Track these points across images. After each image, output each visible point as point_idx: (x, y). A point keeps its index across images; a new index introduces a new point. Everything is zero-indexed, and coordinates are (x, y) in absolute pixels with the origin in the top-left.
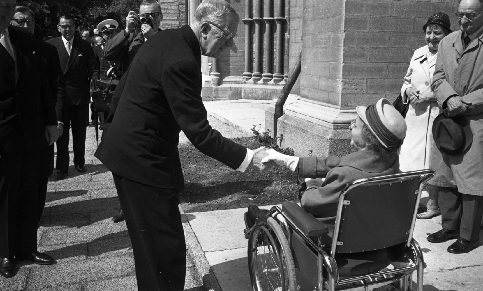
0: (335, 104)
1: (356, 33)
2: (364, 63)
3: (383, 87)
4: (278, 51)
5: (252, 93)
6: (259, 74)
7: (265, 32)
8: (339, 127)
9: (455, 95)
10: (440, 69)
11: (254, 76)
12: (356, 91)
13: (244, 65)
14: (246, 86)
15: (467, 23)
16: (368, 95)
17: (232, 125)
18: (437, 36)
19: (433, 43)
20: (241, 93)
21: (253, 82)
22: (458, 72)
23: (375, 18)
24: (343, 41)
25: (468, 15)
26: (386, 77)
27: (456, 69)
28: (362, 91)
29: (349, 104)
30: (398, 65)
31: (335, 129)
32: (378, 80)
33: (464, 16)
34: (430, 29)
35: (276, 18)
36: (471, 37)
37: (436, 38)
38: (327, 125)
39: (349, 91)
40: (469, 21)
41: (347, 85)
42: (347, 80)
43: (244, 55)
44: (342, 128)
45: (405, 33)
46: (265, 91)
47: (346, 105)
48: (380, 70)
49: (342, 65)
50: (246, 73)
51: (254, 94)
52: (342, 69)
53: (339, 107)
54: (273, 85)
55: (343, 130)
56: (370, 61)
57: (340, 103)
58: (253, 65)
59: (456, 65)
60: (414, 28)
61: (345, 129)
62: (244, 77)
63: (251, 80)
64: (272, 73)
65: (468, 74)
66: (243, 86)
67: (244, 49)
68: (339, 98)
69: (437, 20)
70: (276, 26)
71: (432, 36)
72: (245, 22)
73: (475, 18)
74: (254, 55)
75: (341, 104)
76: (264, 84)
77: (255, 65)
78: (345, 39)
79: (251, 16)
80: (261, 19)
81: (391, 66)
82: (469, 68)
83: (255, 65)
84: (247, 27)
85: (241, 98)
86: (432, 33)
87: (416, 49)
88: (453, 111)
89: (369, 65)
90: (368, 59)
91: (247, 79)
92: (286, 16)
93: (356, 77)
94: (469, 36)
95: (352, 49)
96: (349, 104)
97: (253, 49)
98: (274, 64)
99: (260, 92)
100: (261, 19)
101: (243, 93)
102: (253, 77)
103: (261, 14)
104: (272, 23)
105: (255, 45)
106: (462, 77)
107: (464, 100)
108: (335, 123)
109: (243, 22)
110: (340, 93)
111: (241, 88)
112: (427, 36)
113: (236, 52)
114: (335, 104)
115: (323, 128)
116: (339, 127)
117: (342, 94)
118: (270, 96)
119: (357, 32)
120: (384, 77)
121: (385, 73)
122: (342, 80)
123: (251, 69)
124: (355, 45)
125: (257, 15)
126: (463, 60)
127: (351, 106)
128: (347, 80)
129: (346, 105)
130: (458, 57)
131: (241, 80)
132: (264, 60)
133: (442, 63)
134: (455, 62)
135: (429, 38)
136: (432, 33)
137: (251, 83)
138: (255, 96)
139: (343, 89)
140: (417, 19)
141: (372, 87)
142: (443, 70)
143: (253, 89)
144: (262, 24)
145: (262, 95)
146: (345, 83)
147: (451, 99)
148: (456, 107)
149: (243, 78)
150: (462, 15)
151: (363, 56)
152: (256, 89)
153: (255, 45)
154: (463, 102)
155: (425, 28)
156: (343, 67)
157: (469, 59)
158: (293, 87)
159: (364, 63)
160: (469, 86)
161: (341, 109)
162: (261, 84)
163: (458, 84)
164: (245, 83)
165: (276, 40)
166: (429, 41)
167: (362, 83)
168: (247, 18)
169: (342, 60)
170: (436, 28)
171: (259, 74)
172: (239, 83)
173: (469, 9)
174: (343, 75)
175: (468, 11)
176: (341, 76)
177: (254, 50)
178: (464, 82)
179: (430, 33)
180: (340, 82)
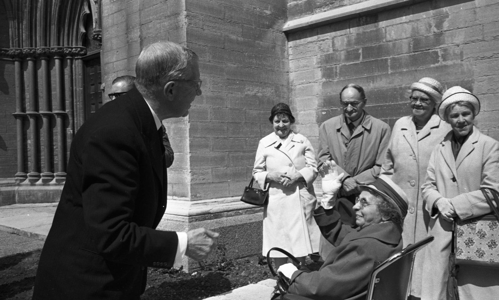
0: (183, 196)
1: (198, 123)
2: (208, 153)
3: (226, 175)
4: (59, 147)
5: (30, 195)
6: (36, 174)
7: (41, 127)
8: (194, 219)
9: (349, 177)
10: (326, 152)
11: (30, 176)
12: (203, 181)
13: (17, 165)
14: (21, 188)
15: (352, 111)
16: (214, 185)
17: (25, 234)
18: (285, 124)
19: (282, 131)
20: (14, 196)
21: (29, 183)
22: (348, 155)
23: (214, 109)
24: (188, 131)
25: (353, 104)
26: (228, 166)
27: (346, 153)
28: (209, 181)
29: (198, 195)
30: (237, 154)
31: (190, 222)
32: (222, 169)
33: (349, 105)
34: (278, 118)
35: (55, 112)
36: (355, 124)
37: (285, 126)
38: (180, 218)
39: (197, 182)
40: (354, 109)
41: (195, 176)
42: (194, 170)
43: (16, 153)
44: (197, 220)
45: (239, 123)
46: (46, 192)
47: (196, 196)
48: (222, 159)
49: (189, 156)
50: (32, 173)
51: (31, 197)
52: (189, 159)
53: (189, 198)
54: (55, 185)
55: (197, 222)
56: (213, 150)
57: (190, 194)
58: (27, 164)
59: (344, 149)
60: (246, 118)
61: (199, 221)
62: (16, 178)
63: (27, 182)
64: (53, 172)
65: (356, 157)
66: (16, 188)
67: (16, 147)
68: (187, 190)
69: (282, 110)
70: (55, 120)
71: (281, 124)
72: (16, 116)
73: (359, 105)
74: (29, 153)
75: (192, 196)
76: (44, 185)
77: (31, 164)
78: (190, 129)
79: (23, 109)
80: (36, 113)
81: (231, 155)
82: (357, 151)
83: (31, 164)
84: (18, 121)
85: (15, 203)
86: (281, 122)
87: (262, 137)
88: (350, 191)
89: (212, 154)
90: (211, 149)
91: (22, 181)
92: (67, 111)
93: (202, 167)
94: (353, 123)
95: (197, 140)
96: (198, 195)
97: (27, 146)
98: (55, 162)
99: (40, 194)
100: (36, 113)
101: (17, 197)
102: (29, 178)
103: (36, 107)
104: (51, 118)
105: (30, 142)
106: (352, 159)
107: (358, 180)
108: (190, 216)
109: (13, 117)
110: (189, 184)
111: (14, 191)
112: (276, 125)
113: (6, 150)
114: (182, 197)
115: (175, 222)
116: (194, 219)
117: (191, 185)
118: (53, 198)
119: (200, 122)
120: (226, 166)
121: (226, 162)
122: (190, 171)
123: (25, 169)
124: (199, 136)
125: (58, 107)
126: (351, 145)
127: (200, 197)
128: (194, 170)
129: (196, 196)
130: (346, 142)
131: (14, 181)
132: (42, 157)
133: (327, 146)
134: (343, 146)
135: (278, 126)
136: (281, 122)
137: (27, 185)
138: (34, 199)
139: (192, 180)
140: (247, 110)
141: (217, 176)
142: (329, 152)
143: (30, 191)
144: (38, 118)
145: (42, 197)
146: (193, 173)
147: (346, 181)
148: (353, 188)
149: (16, 180)
150: (347, 104)
151: (207, 146)
152: (33, 191)
153: (30, 142)
154: (357, 183)
155: (271, 119)
156: (191, 157)
157: (356, 144)
158: (168, 179)
159: (208, 153)
160: (359, 168)
161: (191, 201)
162: (40, 185)
163: (348, 166)
164: (19, 185)
165: (56, 135)
166: (278, 128)
167: (208, 173)
168: (18, 112)
169: (189, 151)
170: (284, 117)
171: (36, 174)
172: (11, 186)
173: (352, 98)
174: (191, 165)
175: (352, 100)
176: (188, 166)
177: (29, 147)
178: (354, 165)
179: (278, 122)
180: (188, 173)
